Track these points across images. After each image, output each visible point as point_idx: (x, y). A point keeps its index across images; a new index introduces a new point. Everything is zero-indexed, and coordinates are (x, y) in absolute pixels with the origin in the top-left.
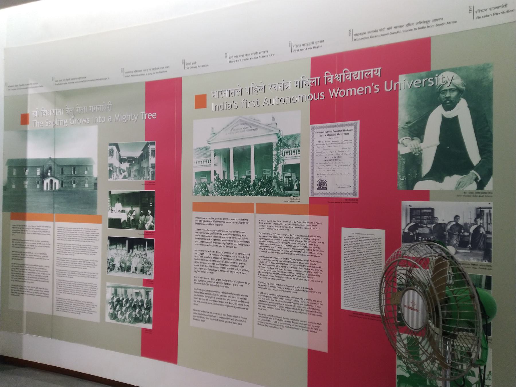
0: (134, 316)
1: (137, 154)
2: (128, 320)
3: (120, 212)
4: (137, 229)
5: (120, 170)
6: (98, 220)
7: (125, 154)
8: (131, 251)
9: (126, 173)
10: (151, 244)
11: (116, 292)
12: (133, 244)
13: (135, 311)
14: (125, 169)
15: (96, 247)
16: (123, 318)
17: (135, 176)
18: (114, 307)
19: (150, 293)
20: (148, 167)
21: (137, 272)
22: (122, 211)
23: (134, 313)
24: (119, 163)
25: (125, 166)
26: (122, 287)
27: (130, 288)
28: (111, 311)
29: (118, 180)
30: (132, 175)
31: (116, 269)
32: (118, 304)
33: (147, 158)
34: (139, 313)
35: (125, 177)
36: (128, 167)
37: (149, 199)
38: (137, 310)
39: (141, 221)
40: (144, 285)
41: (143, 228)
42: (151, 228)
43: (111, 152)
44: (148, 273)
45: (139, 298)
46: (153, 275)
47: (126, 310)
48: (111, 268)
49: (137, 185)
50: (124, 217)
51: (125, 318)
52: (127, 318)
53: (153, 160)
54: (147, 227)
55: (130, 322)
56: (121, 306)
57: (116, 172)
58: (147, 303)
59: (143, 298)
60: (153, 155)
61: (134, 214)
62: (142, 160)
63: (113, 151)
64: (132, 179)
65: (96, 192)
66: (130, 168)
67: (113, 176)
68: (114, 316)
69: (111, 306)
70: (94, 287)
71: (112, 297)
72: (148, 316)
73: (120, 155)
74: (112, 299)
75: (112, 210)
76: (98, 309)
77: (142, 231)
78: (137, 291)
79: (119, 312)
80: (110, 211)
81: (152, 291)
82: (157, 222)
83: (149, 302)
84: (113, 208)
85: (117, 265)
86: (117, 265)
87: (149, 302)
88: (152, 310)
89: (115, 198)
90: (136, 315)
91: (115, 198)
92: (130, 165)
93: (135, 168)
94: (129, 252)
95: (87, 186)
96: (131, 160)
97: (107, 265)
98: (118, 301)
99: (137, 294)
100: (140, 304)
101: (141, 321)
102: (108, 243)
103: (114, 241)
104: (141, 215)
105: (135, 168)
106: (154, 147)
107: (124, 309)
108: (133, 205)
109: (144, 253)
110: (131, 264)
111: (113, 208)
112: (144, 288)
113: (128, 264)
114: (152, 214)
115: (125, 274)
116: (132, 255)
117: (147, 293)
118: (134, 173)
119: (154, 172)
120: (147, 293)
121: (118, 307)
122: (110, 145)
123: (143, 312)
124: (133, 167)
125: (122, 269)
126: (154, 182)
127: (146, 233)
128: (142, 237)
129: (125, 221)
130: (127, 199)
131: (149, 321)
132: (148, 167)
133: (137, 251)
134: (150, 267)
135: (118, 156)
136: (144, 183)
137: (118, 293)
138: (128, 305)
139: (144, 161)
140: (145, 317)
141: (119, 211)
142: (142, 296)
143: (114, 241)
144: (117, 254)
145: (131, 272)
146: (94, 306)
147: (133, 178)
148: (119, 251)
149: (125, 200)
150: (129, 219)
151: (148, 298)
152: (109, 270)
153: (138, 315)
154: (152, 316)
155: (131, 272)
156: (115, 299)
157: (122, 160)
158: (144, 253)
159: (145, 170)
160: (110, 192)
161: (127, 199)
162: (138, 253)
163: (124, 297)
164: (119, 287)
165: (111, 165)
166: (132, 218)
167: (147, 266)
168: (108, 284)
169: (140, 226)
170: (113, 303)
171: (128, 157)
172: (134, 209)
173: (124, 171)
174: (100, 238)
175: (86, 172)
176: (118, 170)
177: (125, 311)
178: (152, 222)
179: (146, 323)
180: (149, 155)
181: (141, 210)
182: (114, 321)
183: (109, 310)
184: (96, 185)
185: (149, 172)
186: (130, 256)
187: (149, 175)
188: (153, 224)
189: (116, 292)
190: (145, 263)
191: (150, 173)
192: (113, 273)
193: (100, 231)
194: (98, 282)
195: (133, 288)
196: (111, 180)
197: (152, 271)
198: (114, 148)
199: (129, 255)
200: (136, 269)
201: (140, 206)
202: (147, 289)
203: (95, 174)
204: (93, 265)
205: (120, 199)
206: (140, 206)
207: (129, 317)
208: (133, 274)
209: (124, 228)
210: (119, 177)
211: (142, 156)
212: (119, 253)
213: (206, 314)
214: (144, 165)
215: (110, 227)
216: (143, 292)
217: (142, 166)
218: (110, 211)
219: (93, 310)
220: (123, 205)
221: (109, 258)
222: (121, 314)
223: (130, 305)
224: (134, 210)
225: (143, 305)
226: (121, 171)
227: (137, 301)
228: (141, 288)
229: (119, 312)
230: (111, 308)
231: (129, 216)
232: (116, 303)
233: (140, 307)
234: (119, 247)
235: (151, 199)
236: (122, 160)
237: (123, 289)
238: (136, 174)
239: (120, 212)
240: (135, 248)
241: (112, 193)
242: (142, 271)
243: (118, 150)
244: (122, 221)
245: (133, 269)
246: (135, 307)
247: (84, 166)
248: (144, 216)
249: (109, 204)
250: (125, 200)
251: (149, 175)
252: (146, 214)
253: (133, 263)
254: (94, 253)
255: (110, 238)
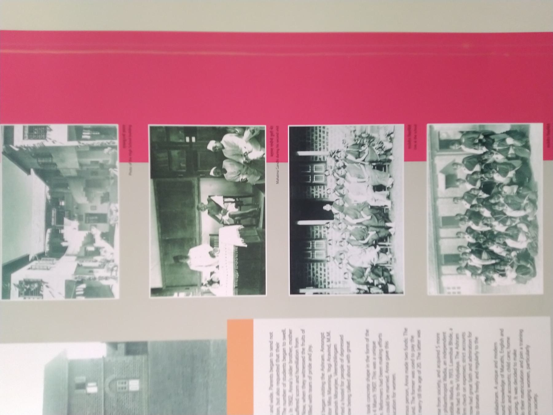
0: (515, 188)
1: (37, 189)
2: (529, 210)
3: (214, 255)
4: (261, 188)
5: (88, 255)
6: (242, 331)
7: (36, 240)
8: (327, 208)
9: (97, 232)
10: (303, 138)
11: (453, 259)
12: (307, 205)
13: (501, 185)
14: (84, 233)
15: (325, 337)
16: (524, 228)
17: (106, 198)
18: (498, 264)
19: (444, 136)
20: (80, 153)
21: (388, 184)
22: (212, 244)
23: (507, 190)
24: (64, 258)
25: (73, 234)
26: (437, 238)
27: (435, 209)
28: (511, 273)
29: (117, 261)
30: (102, 208)
31: (384, 259)
32: (487, 252)
33: (50, 156)
34: (504, 173)
35: (108, 237)
36: (75, 223)
37: (175, 146)
38: (498, 178)
39: (240, 173)
40: (424, 159)
41: (256, 166)
42: (257, 139)
43: (31, 289)
44: (387, 145)
45: (462, 172)
46: (390, 127)
47: (498, 215)
48: (382, 281)
49: (134, 187)
50: (232, 238)
51: (524, 219)
52: (521, 213)
53: (58, 134)
54: (256, 153)
55: (533, 202)
56: (491, 236)
57: (91, 270)
58: (474, 145)
59: (459, 160)
60: (42, 133)
61: (219, 200)
62: (58, 172)
63: (28, 282)
64: (114, 210)
65: (154, 343)
66: (80, 219)
67: (104, 282)
68: (525, 262)
69: (496, 276)
70: (446, 340)
71: (468, 273)
72: (510, 141)
73: (41, 256)
74: (473, 270)
75: (211, 282)
76: (511, 325)
77: (270, 168)
78: (441, 179)
79: (510, 243)
80: (213, 288)
81: (437, 127)
82: (242, 118)
83: (471, 139)
84: (206, 277)
85: (371, 256)
86: (371, 256)
87: (471, 139)
88: (490, 127)
89: (175, 275)
90: (511, 183)
91: (175, 275)
92: (71, 218)
93: (79, 197)
94: (329, 216)
95: (134, 385)
96: (57, 212)
97: (376, 295)
98: (478, 249)
99: (451, 180)
100: (477, 168)
101: (525, 162)
102: (309, 292)
103: (302, 276)
104: (221, 173)
105: (80, 198)
106: (19, 129)
107: (499, 228)
108: (192, 205)
109: (331, 162)
110: (365, 204)
111: (206, 277)
112: (433, 156)
113: (366, 217)
114: (219, 134)
115: (397, 225)
116: (340, 202)
117: (445, 145)
118: (97, 202)
119: (93, 129)
120: (445, 145)
121: (496, 249)
122: (6, 294)
123: (499, 158)
124: (78, 207)
125: (382, 241)
126: (123, 129)
127: (275, 156)
128: (285, 168)
129: (242, 235)
130: (175, 225)
131: (521, 135)
132: (80, 153)
133: (327, 188)
134: (370, 138)
135: (42, 263)
136: (126, 165)
137: (455, 252)
138: (486, 213)
139: (60, 166)
140: (511, 151)
141: (212, 255)
142: (454, 164)
143: (302, 276)
144: (340, 257)
145: (388, 203)
146: (503, 344)
147: (113, 207)
148: (333, 250)
149: (180, 234)
150: (236, 219)
151: (459, 142)
152: (391, 288)
153: (511, 174)
154: (507, 126)
155: (388, 203)
156: (475, 261)
157: (57, 250)
158: (331, 162)
159: (88, 161)
160: (155, 291)
161: (175, 225)
162: (331, 184)
163: (463, 227)
164: (437, 248)
165: (70, 289)
166: (232, 208)
167: (365, 149)
168: (432, 290)
169: (253, 180)
170: (486, 268)
171: (48, 224)
172: (204, 200)
173: (91, 239)
174: (294, 325)
175: (92, 389)
176: (86, 264)
177: (503, 222)
178: (241, 135)
179: (527, 146)
180: (44, 148)
181: (207, 175)
182: (539, 260)
183: (507, 283)
184: (132, 348)
185: (93, 148)
186: (341, 209)
187: (102, 148)
188: (247, 133)
189: (453, 259)
190: (358, 156)
191: (97, 143)
192: (399, 272)
193: (277, 323)
194: (431, 327)
195: (435, 198)
196: (116, 290)
197: (380, 131)
198: (17, 276)
199: (341, 216)
200: (379, 188)
201: (194, 180)
202: (432, 147)
203: (95, 351)
204: (378, 348)
205: (176, 252)
206: (194, 180)
207: (518, 208)
208: (393, 196)
209: (262, 234)
210: (109, 257)
211: (45, 174)
212: (339, 249)
213: (345, 363)
214: (70, 164)
215: (262, 291)
216: (443, 160)
217: (74, 173)
218: (213, 289)
219: (515, 345)
220: (191, 241)
221: (354, 287)
222: (514, 237)
223: (485, 203)
224: (210, 200)
225: (479, 159)
226: (91, 249)
227: (471, 179)
228: (433, 166)
229: (510, 243)
230: (503, 274)
231: (226, 218)
232: (485, 255)
233: (488, 168)
234: (321, 250)
235: (173, 138)
236: (57, 250)
237: (444, 232)
238: (99, 193)
239: (214, 255)
240: (318, 193)
241: (158, 284)
242: (381, 165)
243: (23, 261)
244: (241, 243)
245: (380, 199)
246: (488, 187)
247: (70, 397)
248: (226, 164)
249: (194, 296)
250: (180, 234)
251: (102, 148)
252: (219, 156)
253: (361, 199)
254: (345, 347)
255: (294, 290)
